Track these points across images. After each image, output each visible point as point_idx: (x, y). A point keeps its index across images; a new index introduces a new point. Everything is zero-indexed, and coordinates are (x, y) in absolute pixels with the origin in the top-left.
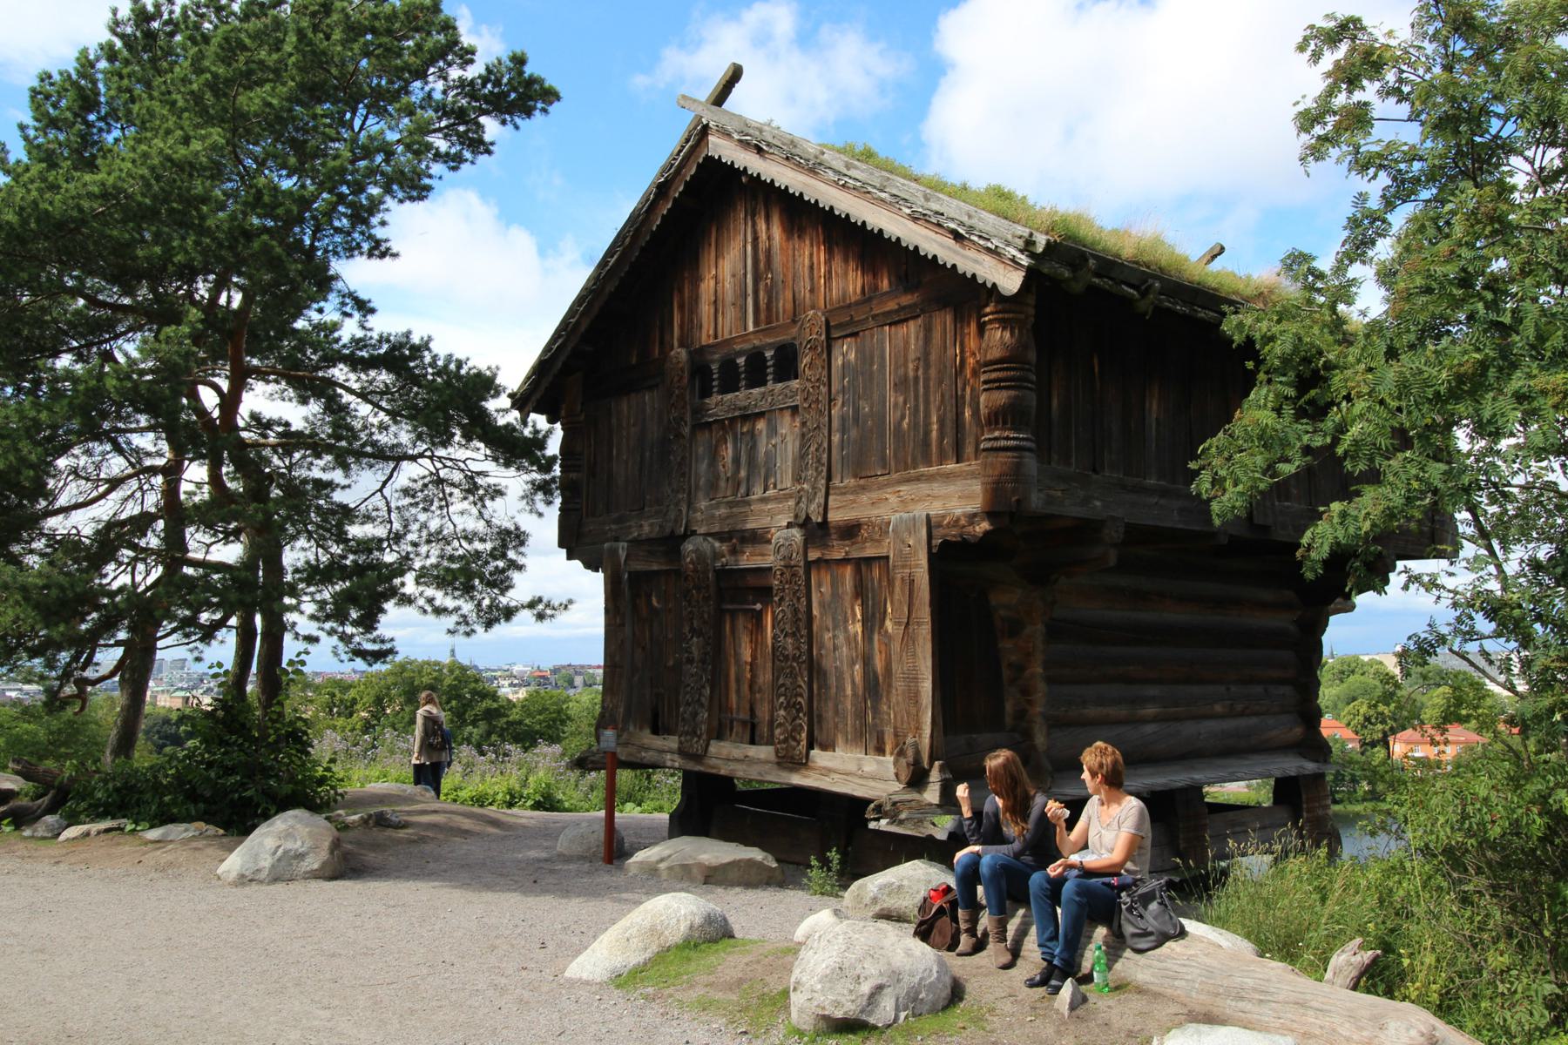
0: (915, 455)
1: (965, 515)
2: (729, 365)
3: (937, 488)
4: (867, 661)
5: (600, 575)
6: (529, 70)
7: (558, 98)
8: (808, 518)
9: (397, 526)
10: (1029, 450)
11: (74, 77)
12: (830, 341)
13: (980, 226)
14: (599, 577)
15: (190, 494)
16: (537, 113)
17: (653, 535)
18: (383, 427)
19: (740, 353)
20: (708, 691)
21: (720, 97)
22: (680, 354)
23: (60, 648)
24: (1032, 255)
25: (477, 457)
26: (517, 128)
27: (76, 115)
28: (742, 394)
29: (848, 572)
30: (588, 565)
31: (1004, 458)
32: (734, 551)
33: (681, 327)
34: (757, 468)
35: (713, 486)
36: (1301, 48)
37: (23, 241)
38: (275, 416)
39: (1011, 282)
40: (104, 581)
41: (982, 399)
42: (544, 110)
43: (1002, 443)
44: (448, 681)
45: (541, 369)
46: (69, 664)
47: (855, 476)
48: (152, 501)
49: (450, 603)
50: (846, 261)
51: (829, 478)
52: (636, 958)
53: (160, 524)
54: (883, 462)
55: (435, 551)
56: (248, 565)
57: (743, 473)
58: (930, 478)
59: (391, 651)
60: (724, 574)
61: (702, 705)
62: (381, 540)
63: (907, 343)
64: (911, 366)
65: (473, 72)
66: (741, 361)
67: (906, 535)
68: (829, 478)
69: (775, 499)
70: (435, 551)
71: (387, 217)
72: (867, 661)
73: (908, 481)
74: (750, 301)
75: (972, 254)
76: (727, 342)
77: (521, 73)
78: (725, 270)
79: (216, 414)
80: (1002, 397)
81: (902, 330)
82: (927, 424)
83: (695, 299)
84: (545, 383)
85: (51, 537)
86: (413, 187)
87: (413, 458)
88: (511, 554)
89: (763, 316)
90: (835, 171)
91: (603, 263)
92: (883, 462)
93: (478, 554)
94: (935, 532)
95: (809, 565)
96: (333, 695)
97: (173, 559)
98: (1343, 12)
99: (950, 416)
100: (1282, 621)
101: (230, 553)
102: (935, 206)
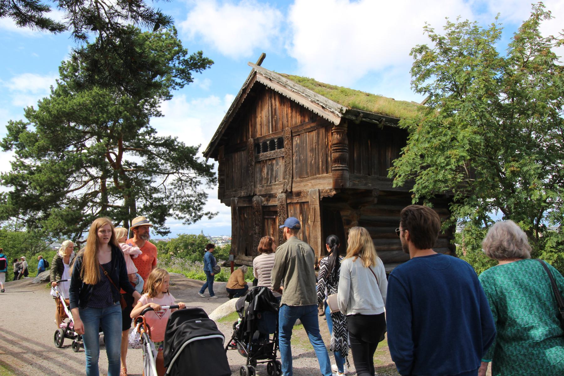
0: (315, 171)
2: (265, 143)
3: (321, 181)
6: (204, 56)
7: (213, 63)
8: (287, 190)
9: (168, 194)
11: (72, 62)
12: (292, 136)
13: (329, 104)
14: (230, 208)
15: (109, 185)
16: (207, 68)
18: (162, 164)
19: (268, 140)
21: (260, 64)
22: (251, 140)
23: (72, 232)
24: (342, 114)
25: (192, 173)
26: (201, 73)
27: (72, 74)
28: (268, 153)
29: (298, 206)
30: (227, 205)
31: (338, 172)
32: (268, 200)
33: (252, 132)
34: (273, 177)
35: (261, 180)
36: (411, 54)
37: (58, 118)
38: (132, 162)
39: (337, 121)
40: (85, 212)
42: (209, 67)
43: (338, 168)
44: (198, 242)
45: (212, 144)
46: (74, 237)
47: (300, 178)
48: (97, 188)
49: (183, 216)
50: (296, 112)
51: (293, 178)
52: (224, 314)
53: (100, 194)
54: (307, 173)
55: (179, 200)
56: (125, 208)
57: (269, 177)
58: (320, 178)
59: (169, 232)
60: (265, 207)
62: (163, 198)
63: (313, 138)
64: (314, 145)
65: (187, 57)
66: (268, 142)
68: (293, 178)
69: (278, 184)
70: (179, 200)
71: (160, 105)
73: (314, 179)
75: (327, 112)
76: (264, 137)
77: (201, 57)
78: (263, 115)
79: (115, 161)
80: (337, 155)
82: (319, 162)
83: (255, 123)
84: (213, 149)
85: (68, 199)
86: (167, 96)
87: (173, 173)
88: (203, 201)
89: (274, 129)
90: (291, 87)
91: (228, 113)
92: (307, 173)
93: (191, 201)
94: (321, 194)
95: (287, 204)
96: (161, 247)
97: (104, 205)
98: (421, 44)
99: (325, 160)
101: (120, 203)
102: (317, 99)
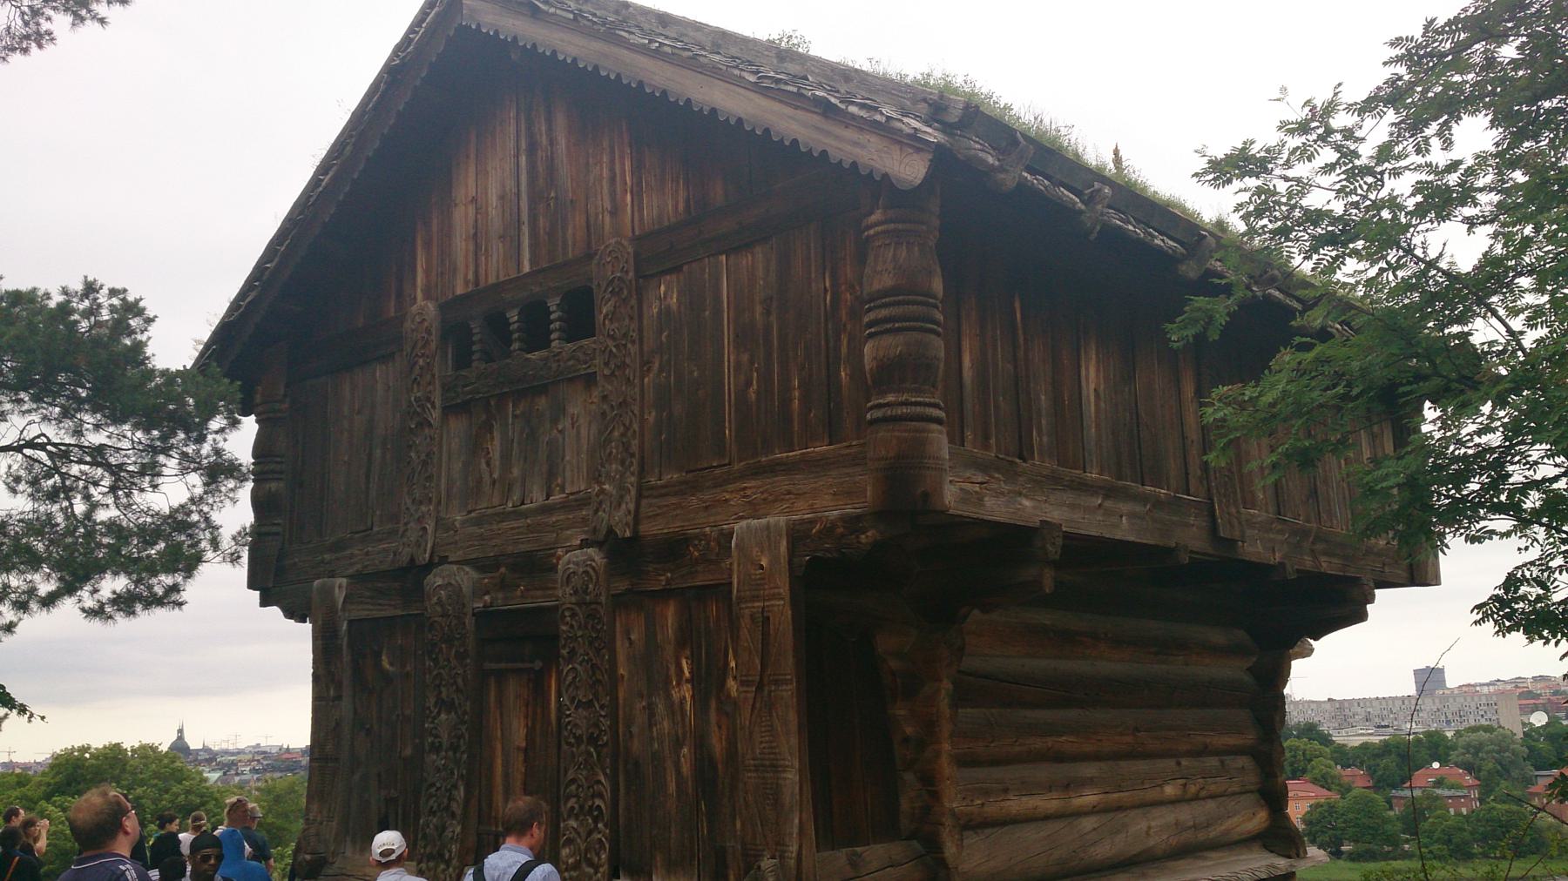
1: (845, 519)
4: (701, 744)
5: (307, 627)
8: (610, 531)
10: (939, 421)
17: (384, 567)
20: (461, 793)
22: (424, 308)
30: (290, 613)
41: (868, 349)
57: (516, 472)
58: (788, 468)
61: (453, 815)
66: (513, 316)
67: (755, 551)
72: (701, 744)
74: (525, 229)
81: (745, 260)
83: (447, 232)
100: (1233, 670)
